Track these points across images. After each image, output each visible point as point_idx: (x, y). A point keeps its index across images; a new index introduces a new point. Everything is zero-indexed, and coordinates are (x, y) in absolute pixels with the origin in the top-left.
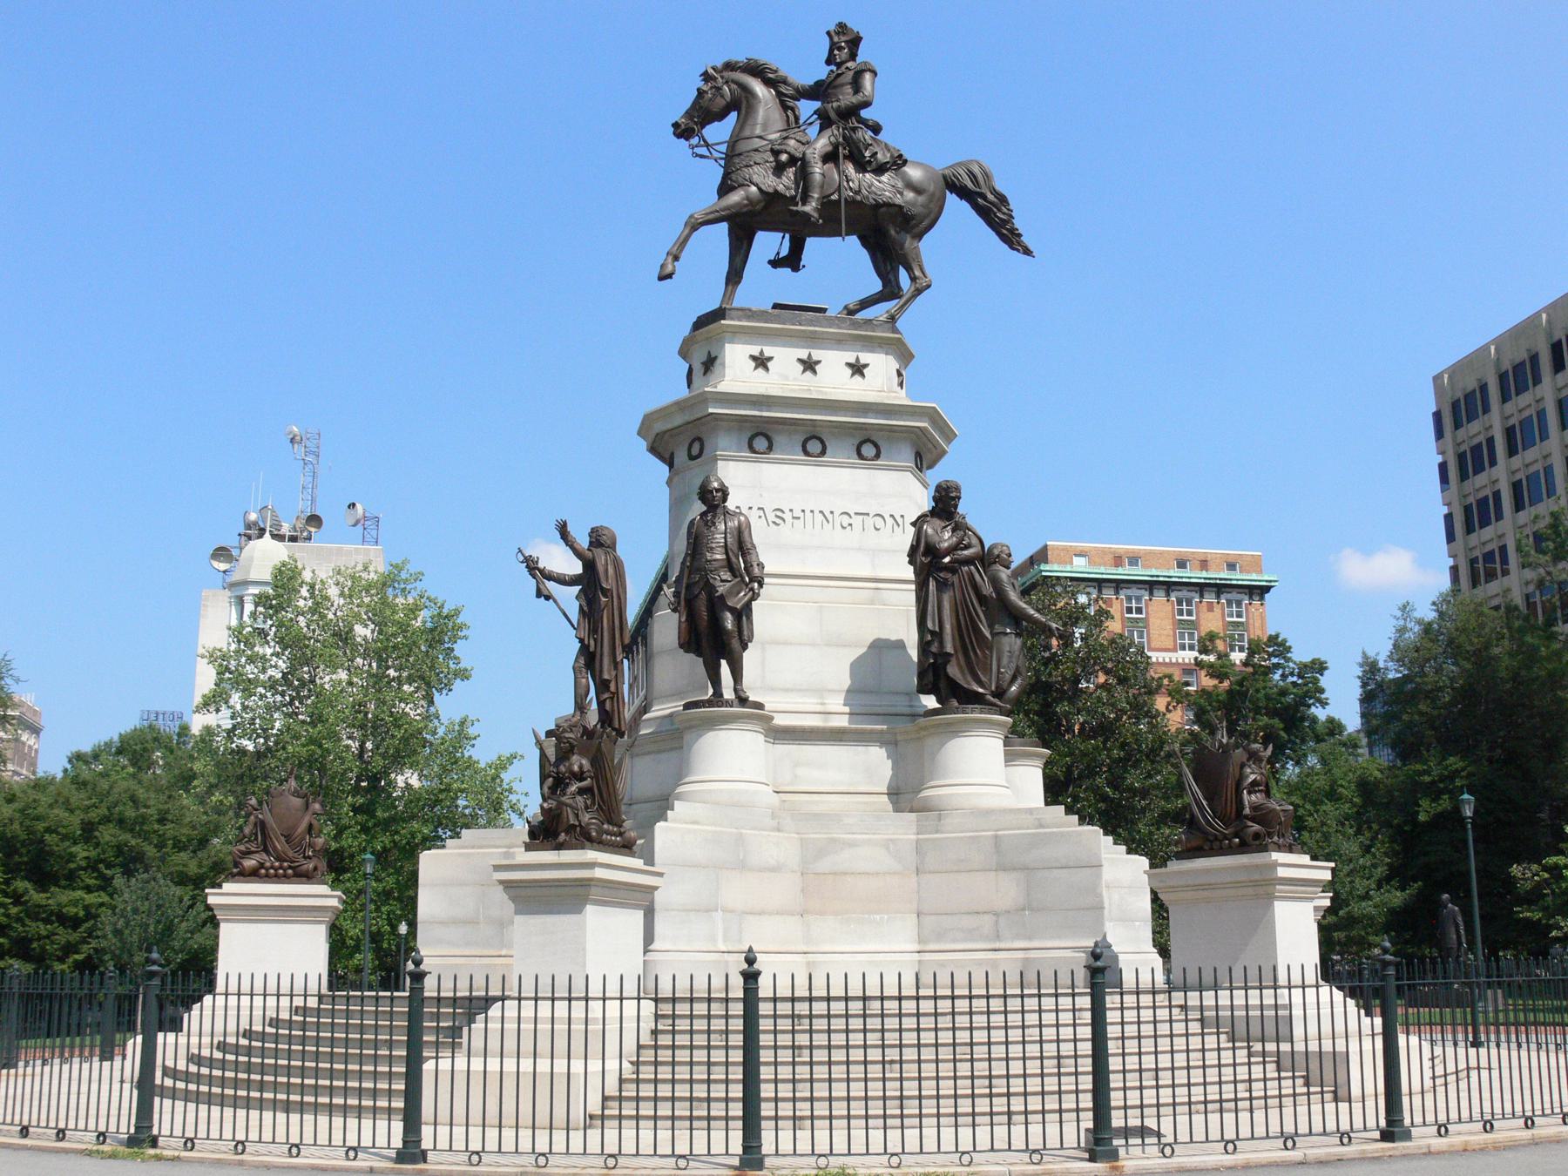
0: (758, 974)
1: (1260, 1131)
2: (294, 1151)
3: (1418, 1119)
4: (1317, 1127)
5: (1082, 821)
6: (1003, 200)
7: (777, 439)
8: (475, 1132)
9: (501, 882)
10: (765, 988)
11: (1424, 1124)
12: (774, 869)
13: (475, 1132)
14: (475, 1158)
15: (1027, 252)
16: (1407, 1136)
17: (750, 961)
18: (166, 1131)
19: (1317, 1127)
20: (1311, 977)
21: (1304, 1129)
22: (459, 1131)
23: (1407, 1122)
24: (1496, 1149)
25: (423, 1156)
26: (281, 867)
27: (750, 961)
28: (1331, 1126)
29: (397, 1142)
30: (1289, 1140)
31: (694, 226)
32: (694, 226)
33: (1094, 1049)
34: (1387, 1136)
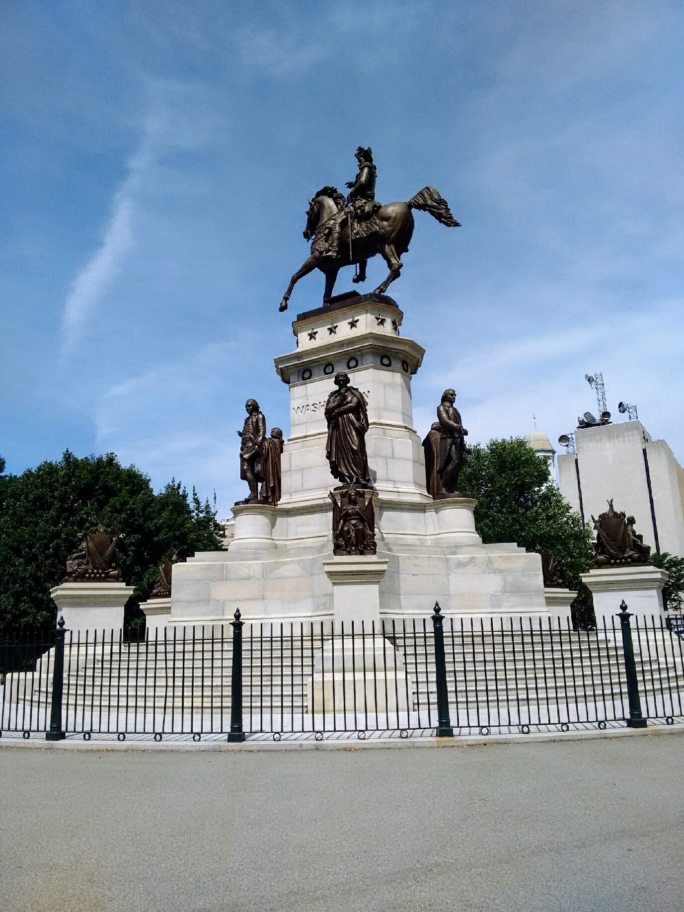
0: (242, 624)
1: (340, 726)
2: (87, 736)
3: (652, 713)
4: (178, 729)
5: (528, 550)
6: (441, 202)
7: (313, 371)
8: (361, 716)
9: (328, 573)
10: (245, 633)
11: (9, 729)
12: (247, 578)
13: (361, 716)
14: (197, 737)
15: (457, 225)
16: (62, 736)
17: (437, 610)
18: (652, 713)
19: (140, 728)
20: (116, 638)
21: (168, 729)
22: (350, 716)
23: (644, 715)
24: (497, 743)
25: (643, 724)
26: (98, 573)
27: (437, 610)
28: (592, 717)
29: (227, 728)
30: (197, 735)
31: (294, 281)
32: (294, 281)
33: (241, 672)
34: (49, 737)
